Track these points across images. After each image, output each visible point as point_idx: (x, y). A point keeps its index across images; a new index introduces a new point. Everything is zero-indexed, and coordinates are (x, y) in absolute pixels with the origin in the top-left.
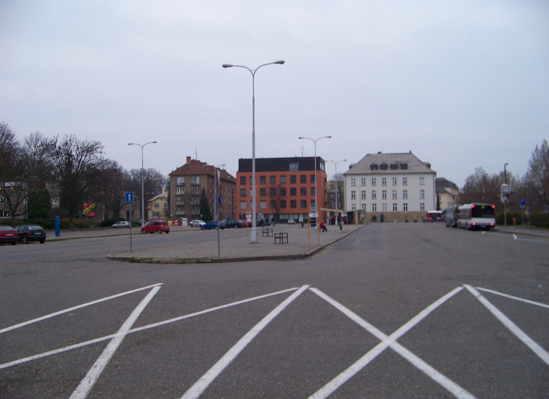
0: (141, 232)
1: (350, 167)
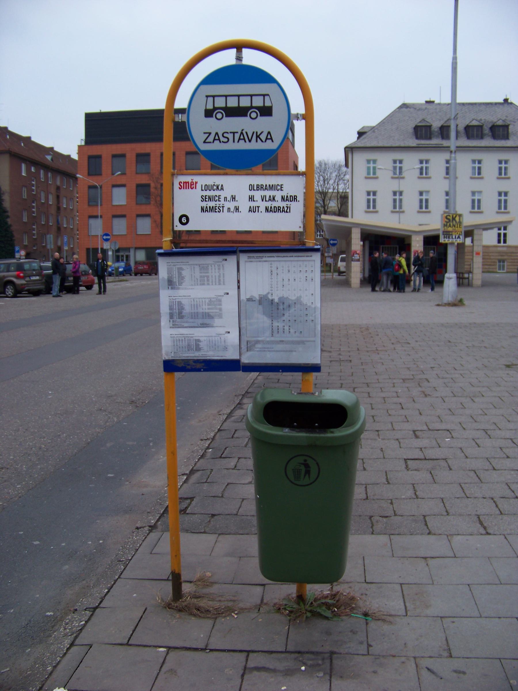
1: (361, 134)
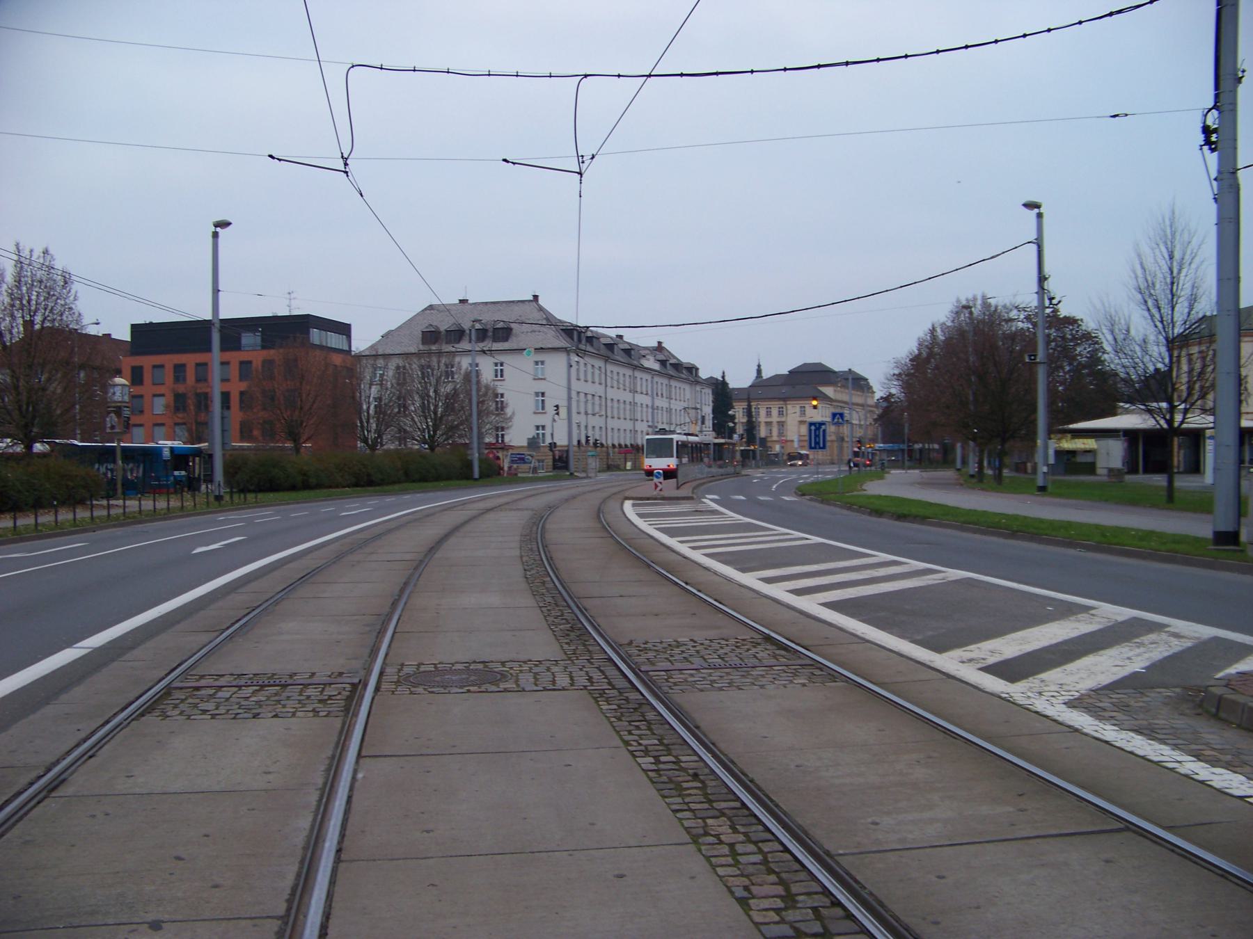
0: (670, 747)
